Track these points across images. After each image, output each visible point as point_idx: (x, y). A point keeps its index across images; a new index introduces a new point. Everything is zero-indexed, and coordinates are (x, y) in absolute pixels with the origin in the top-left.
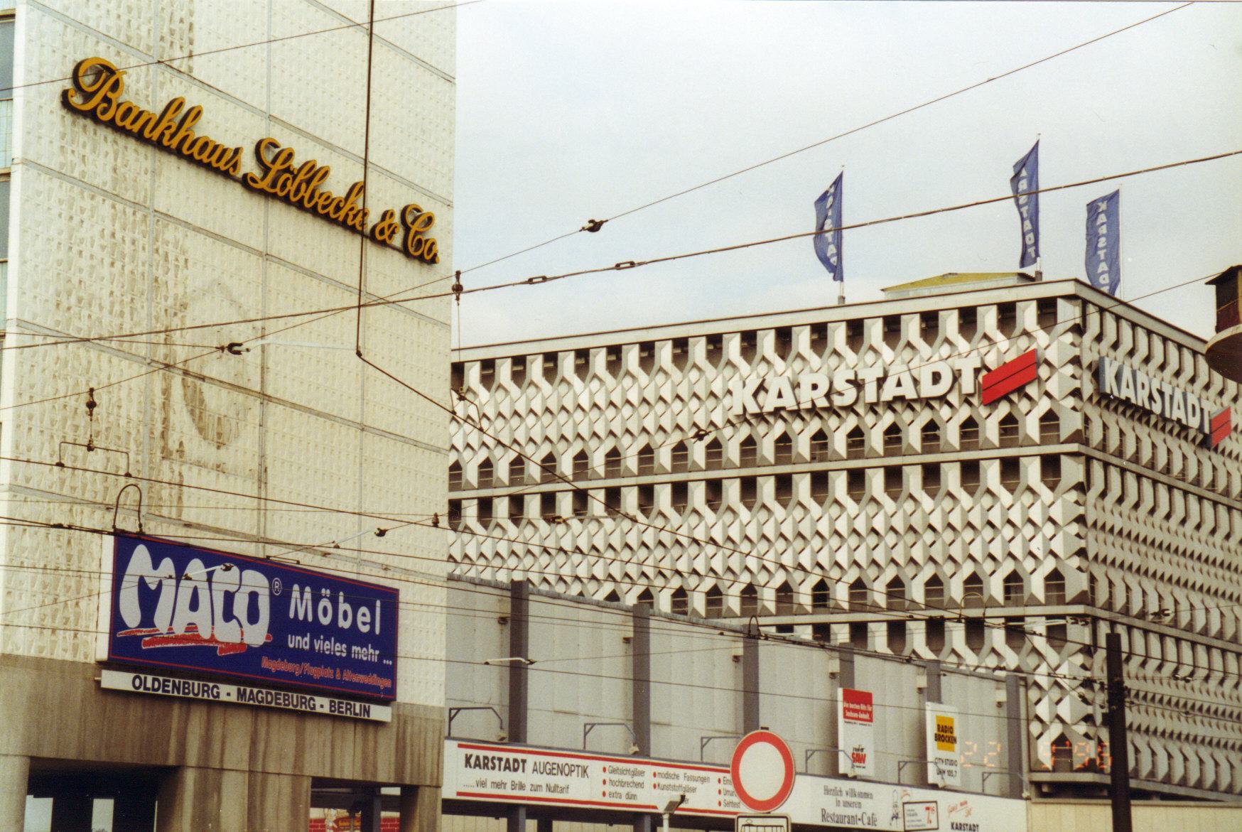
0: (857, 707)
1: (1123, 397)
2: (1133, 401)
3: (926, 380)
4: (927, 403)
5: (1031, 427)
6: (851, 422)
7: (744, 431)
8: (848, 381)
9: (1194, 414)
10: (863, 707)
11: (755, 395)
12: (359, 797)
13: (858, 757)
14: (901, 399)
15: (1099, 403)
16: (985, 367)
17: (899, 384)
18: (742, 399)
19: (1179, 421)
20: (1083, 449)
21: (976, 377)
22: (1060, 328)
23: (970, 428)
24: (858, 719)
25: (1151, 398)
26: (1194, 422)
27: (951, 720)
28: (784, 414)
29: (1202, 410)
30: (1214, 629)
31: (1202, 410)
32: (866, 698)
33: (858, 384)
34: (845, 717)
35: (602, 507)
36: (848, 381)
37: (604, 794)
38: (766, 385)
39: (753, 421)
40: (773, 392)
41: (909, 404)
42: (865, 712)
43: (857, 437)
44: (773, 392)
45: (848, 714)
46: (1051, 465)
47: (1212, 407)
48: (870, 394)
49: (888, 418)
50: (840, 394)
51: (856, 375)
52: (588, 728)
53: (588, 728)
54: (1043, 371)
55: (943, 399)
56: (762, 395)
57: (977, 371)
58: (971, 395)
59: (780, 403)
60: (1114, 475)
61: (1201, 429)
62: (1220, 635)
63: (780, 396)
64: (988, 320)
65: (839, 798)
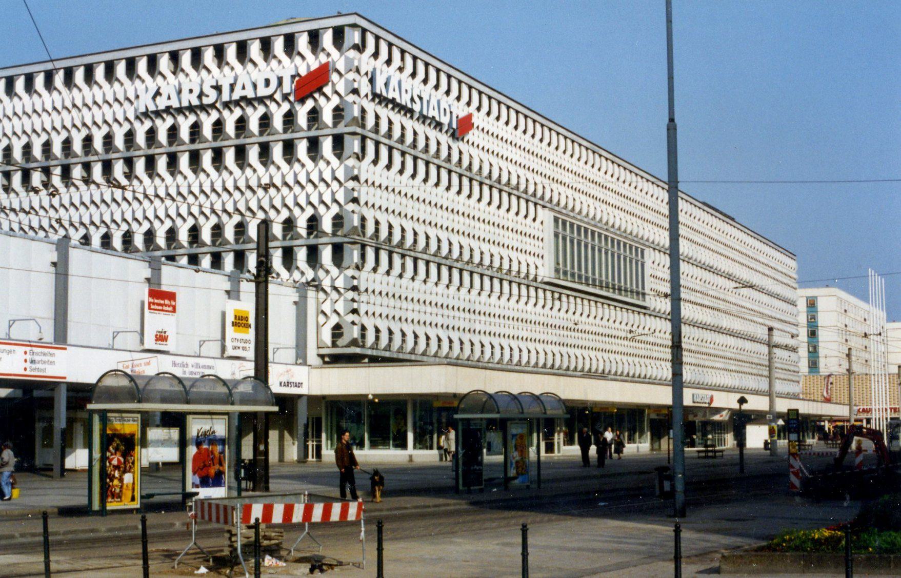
0: (162, 302)
1: (390, 97)
2: (398, 101)
4: (261, 100)
5: (327, 117)
6: (215, 115)
7: (148, 124)
8: (212, 87)
9: (445, 114)
10: (167, 302)
11: (154, 98)
13: (161, 337)
14: (243, 98)
15: (373, 100)
16: (299, 75)
17: (244, 88)
18: (146, 102)
19: (434, 118)
20: (359, 130)
21: (292, 82)
23: (289, 118)
24: (162, 310)
25: (412, 100)
26: (445, 120)
27: (248, 312)
28: (172, 111)
29: (451, 113)
31: (451, 113)
32: (171, 296)
33: (218, 88)
34: (150, 308)
35: (59, 178)
36: (212, 87)
37: (25, 369)
38: (161, 91)
39: (153, 116)
40: (165, 96)
41: (249, 102)
42: (169, 306)
43: (218, 126)
44: (165, 96)
45: (153, 307)
47: (461, 110)
48: (225, 97)
49: (238, 112)
50: (207, 96)
51: (217, 82)
52: (115, 335)
53: (115, 335)
54: (334, 77)
55: (271, 97)
56: (158, 99)
57: (293, 77)
58: (289, 94)
59: (169, 103)
61: (450, 124)
63: (169, 98)
64: (303, 43)
65: (185, 369)
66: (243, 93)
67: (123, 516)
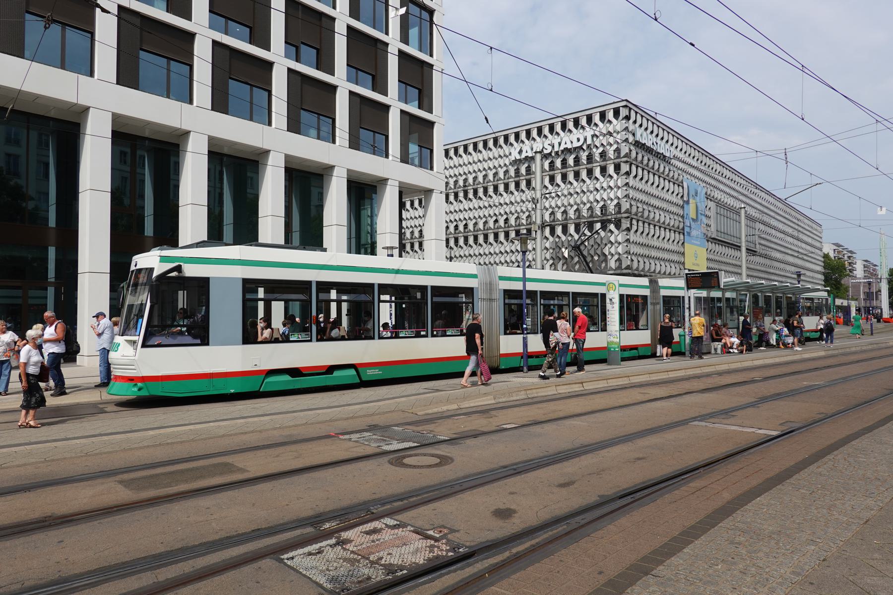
3: (575, 141)
12: (716, 592)
14: (566, 149)
18: (515, 155)
22: (621, 118)
30: (662, 221)
46: (617, 168)
60: (640, 170)
62: (664, 223)
66: (566, 146)
67: (118, 518)
